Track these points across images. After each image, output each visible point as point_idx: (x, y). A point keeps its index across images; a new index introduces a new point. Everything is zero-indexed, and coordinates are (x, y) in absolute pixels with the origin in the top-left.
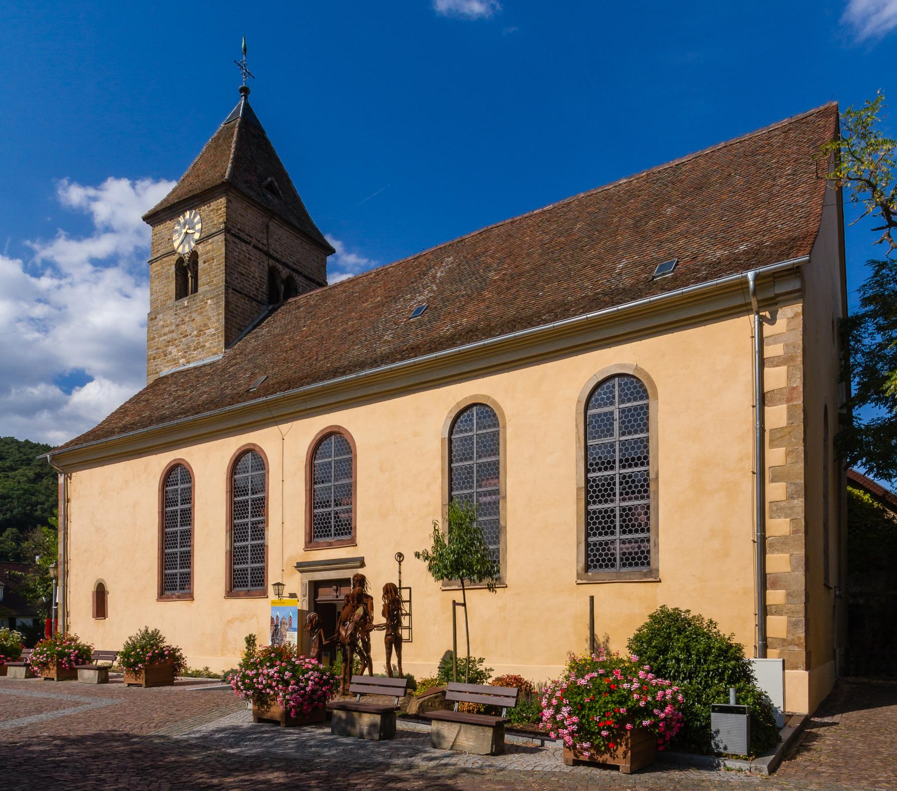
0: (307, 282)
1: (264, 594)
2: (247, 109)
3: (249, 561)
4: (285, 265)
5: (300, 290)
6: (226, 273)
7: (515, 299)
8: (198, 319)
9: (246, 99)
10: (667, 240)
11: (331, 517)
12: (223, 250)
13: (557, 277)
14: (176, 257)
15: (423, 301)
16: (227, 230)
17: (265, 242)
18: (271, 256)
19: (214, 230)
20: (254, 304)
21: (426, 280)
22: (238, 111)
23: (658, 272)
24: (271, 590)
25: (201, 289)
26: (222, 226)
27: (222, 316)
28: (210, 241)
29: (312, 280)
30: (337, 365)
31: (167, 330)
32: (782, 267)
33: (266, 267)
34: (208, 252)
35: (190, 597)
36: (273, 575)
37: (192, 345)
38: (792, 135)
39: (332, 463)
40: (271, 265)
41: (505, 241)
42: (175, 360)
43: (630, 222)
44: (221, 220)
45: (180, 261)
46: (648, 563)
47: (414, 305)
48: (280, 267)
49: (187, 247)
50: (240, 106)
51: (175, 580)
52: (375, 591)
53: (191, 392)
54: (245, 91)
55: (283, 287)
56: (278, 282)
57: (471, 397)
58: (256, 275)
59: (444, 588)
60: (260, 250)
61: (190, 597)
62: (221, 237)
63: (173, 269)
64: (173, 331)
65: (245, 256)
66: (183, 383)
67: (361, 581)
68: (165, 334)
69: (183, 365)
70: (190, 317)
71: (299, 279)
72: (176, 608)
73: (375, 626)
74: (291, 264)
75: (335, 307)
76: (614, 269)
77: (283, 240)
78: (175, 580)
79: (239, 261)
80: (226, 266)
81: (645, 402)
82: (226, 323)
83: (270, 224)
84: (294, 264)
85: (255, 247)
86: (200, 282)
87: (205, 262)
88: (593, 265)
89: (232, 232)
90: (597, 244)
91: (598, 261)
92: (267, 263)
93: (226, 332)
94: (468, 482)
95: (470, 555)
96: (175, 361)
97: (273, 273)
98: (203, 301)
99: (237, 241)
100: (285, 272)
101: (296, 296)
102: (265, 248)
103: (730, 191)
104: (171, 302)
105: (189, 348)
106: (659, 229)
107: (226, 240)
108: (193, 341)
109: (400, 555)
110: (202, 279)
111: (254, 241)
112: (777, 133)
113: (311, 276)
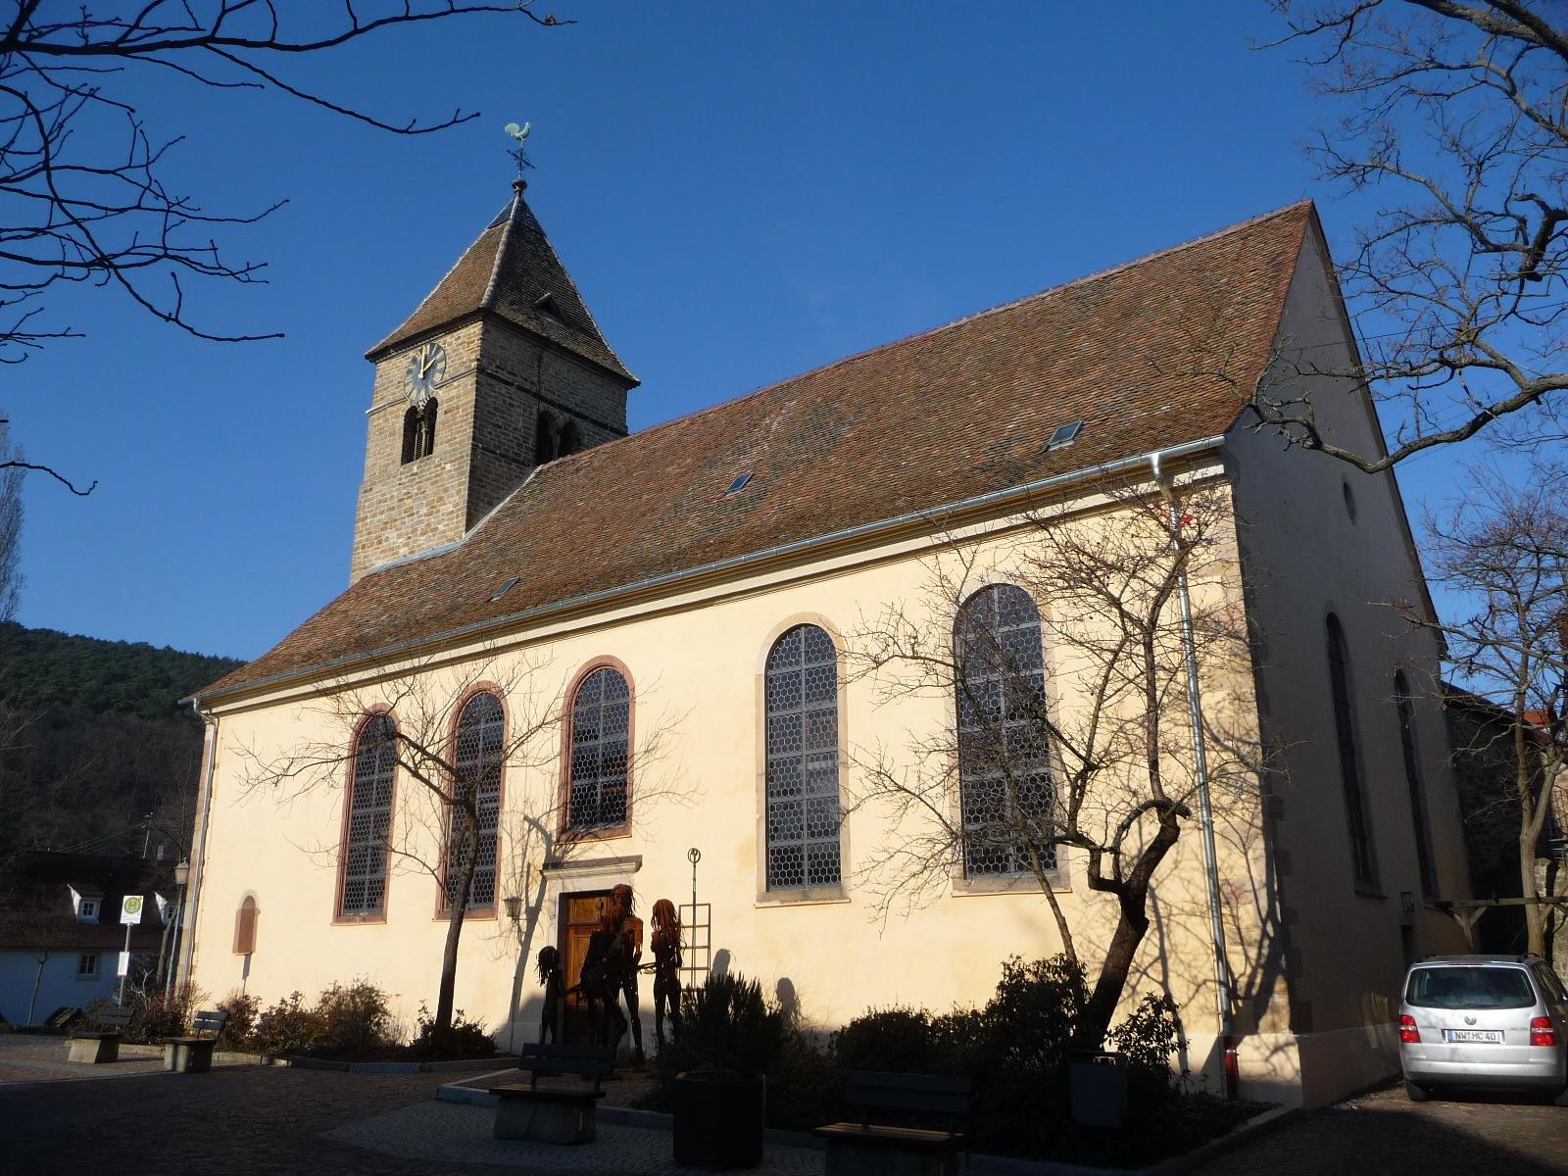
1: (492, 914)
3: (367, 885)
4: (564, 408)
5: (585, 441)
7: (870, 469)
8: (430, 490)
9: (520, 196)
11: (598, 795)
12: (473, 396)
13: (928, 439)
14: (406, 406)
15: (747, 467)
17: (535, 379)
19: (463, 371)
21: (758, 433)
23: (1053, 441)
24: (502, 907)
25: (436, 449)
26: (474, 364)
28: (455, 384)
29: (604, 426)
30: (616, 563)
31: (384, 506)
32: (1191, 448)
34: (452, 399)
35: (843, 896)
36: (507, 884)
37: (420, 528)
40: (542, 410)
41: (870, 379)
42: (392, 549)
43: (1032, 360)
44: (473, 357)
45: (412, 411)
46: (1055, 866)
47: (734, 473)
48: (555, 411)
49: (423, 392)
50: (512, 204)
51: (361, 891)
53: (410, 599)
54: (522, 185)
55: (558, 438)
56: (552, 431)
57: (796, 616)
58: (520, 426)
59: (758, 905)
60: (527, 391)
62: (471, 380)
63: (401, 422)
64: (393, 509)
65: (505, 402)
66: (400, 584)
68: (382, 513)
69: (403, 554)
71: (583, 426)
73: (643, 967)
75: (628, 472)
77: (558, 377)
78: (361, 891)
80: (475, 417)
81: (1035, 624)
82: (470, 495)
83: (545, 354)
84: (577, 405)
85: (519, 388)
86: (437, 440)
87: (446, 413)
88: (976, 424)
89: (487, 373)
90: (987, 391)
91: (985, 417)
92: (536, 407)
93: (469, 508)
94: (795, 740)
97: (544, 420)
99: (494, 382)
100: (562, 418)
101: (579, 450)
102: (535, 389)
103: (1164, 322)
104: (396, 466)
105: (414, 531)
107: (477, 382)
108: (421, 522)
109: (695, 852)
111: (518, 381)
112: (1234, 239)
113: (601, 420)
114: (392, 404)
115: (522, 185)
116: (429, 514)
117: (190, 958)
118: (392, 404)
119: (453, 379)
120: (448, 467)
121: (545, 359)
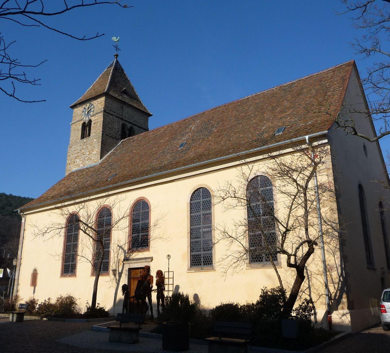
0: (139, 129)
1: (108, 274)
2: (117, 62)
4: (130, 123)
5: (136, 132)
6: (103, 128)
8: (89, 147)
9: (116, 59)
10: (92, 231)
11: (140, 239)
12: (102, 119)
14: (82, 122)
15: (184, 140)
16: (104, 111)
17: (121, 114)
18: (123, 120)
19: (99, 111)
20: (114, 140)
21: (188, 130)
22: (113, 63)
23: (276, 132)
24: (111, 272)
25: (91, 135)
26: (103, 109)
27: (100, 144)
28: (97, 115)
29: (142, 128)
31: (76, 152)
33: (121, 123)
35: (213, 269)
36: (112, 265)
37: (86, 159)
38: (336, 73)
39: (140, 213)
42: (78, 165)
43: (270, 108)
44: (102, 107)
45: (84, 123)
47: (180, 142)
49: (87, 118)
51: (69, 268)
52: (153, 273)
54: (117, 55)
55: (128, 131)
56: (126, 129)
59: (188, 272)
61: (213, 269)
62: (102, 114)
64: (78, 153)
66: (81, 175)
67: (148, 269)
70: (86, 147)
71: (135, 128)
72: (68, 280)
73: (153, 290)
74: (132, 122)
76: (261, 129)
77: (127, 113)
78: (69, 268)
79: (109, 123)
80: (103, 125)
81: (271, 187)
86: (91, 132)
87: (94, 124)
88: (253, 127)
91: (256, 125)
92: (121, 122)
93: (101, 152)
94: (199, 222)
95: (201, 257)
96: (78, 165)
97: (123, 126)
98: (92, 140)
99: (109, 115)
100: (129, 126)
101: (134, 135)
102: (121, 117)
103: (310, 97)
105: (85, 159)
106: (281, 112)
107: (103, 115)
108: (87, 157)
109: (169, 256)
110: (93, 130)
111: (116, 114)
112: (331, 72)
113: (141, 126)
114: (78, 121)
115: (117, 55)
116: (89, 154)
117: (17, 288)
118: (78, 121)
119: (96, 114)
120: (95, 140)
121: (124, 108)
